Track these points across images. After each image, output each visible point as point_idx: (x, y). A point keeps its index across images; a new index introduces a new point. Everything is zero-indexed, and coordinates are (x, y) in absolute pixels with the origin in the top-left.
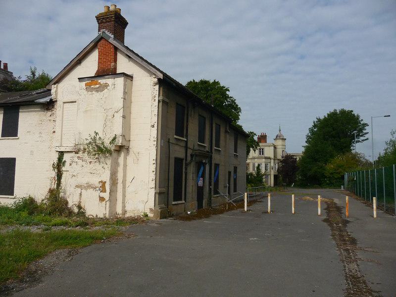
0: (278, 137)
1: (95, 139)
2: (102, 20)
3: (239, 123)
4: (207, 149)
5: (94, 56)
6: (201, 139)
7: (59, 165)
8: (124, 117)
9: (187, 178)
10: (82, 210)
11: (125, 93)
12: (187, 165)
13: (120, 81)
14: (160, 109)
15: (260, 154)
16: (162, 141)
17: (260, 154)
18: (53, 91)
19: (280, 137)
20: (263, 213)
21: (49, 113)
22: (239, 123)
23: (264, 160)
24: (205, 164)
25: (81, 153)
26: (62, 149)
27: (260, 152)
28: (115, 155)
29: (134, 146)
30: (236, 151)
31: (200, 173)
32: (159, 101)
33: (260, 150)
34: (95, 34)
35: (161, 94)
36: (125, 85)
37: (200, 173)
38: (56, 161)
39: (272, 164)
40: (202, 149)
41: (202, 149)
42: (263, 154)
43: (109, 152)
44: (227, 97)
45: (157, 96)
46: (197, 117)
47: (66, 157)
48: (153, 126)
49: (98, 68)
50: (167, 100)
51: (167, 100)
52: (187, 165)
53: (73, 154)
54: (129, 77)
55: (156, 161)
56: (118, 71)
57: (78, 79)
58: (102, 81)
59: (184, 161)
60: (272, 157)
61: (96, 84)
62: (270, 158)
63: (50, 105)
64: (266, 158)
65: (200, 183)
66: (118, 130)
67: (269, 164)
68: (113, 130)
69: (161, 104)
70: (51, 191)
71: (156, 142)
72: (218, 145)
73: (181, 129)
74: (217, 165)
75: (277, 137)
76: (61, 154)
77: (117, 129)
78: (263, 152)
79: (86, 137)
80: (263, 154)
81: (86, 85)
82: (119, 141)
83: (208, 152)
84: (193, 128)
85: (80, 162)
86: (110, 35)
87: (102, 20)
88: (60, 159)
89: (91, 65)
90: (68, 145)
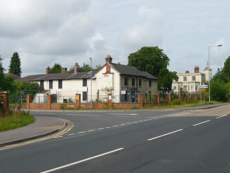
0: (206, 69)
1: (106, 88)
2: (107, 59)
5: (105, 68)
6: (133, 84)
7: (98, 93)
8: (112, 83)
10: (140, 62)
11: (113, 77)
13: (112, 74)
15: (193, 80)
17: (193, 80)
18: (96, 75)
19: (207, 68)
21: (95, 81)
24: (135, 92)
25: (103, 91)
26: (99, 90)
27: (193, 79)
28: (111, 91)
29: (115, 89)
31: (133, 94)
33: (193, 77)
34: (105, 63)
37: (133, 94)
38: (97, 92)
42: (195, 80)
43: (110, 90)
44: (162, 54)
46: (131, 79)
47: (99, 91)
50: (122, 78)
51: (122, 78)
53: (101, 91)
56: (111, 72)
58: (107, 75)
60: (200, 81)
62: (199, 83)
63: (95, 79)
64: (196, 82)
65: (133, 97)
66: (111, 86)
68: (110, 86)
70: (96, 99)
72: (140, 85)
73: (126, 84)
75: (206, 68)
76: (98, 91)
77: (111, 85)
78: (195, 79)
79: (105, 87)
80: (195, 80)
82: (112, 88)
84: (130, 82)
87: (107, 59)
88: (98, 92)
89: (104, 70)
90: (100, 88)
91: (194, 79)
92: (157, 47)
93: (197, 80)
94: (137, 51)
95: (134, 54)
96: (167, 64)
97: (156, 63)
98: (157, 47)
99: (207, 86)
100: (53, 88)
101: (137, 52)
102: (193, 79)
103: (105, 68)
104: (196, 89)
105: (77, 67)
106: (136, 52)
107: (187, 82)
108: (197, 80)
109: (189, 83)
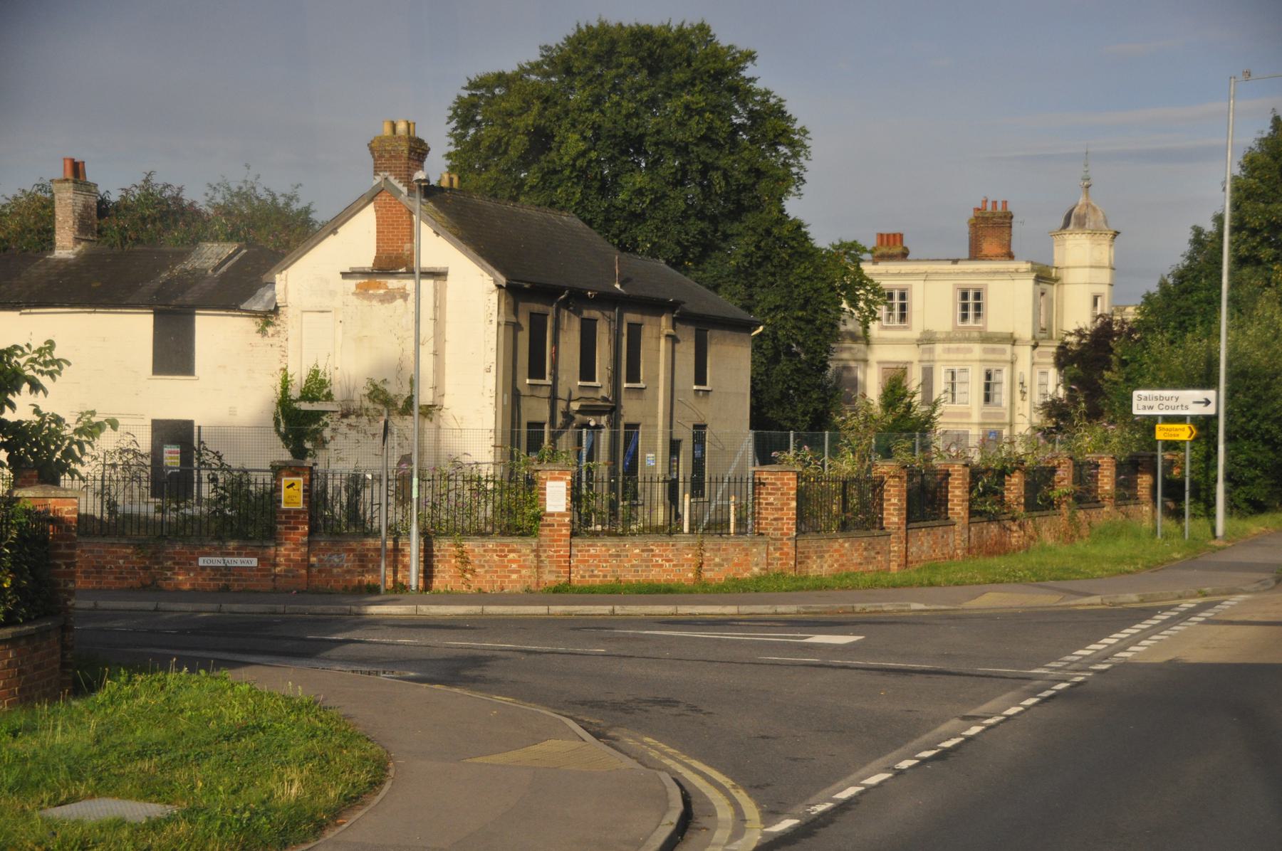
3: (793, 207)
4: (604, 393)
5: (366, 220)
8: (435, 354)
9: (443, 630)
12: (555, 437)
13: (427, 285)
14: (501, 338)
15: (965, 317)
16: (506, 396)
20: (220, 367)
22: (793, 207)
23: (977, 350)
30: (700, 378)
32: (499, 324)
35: (502, 310)
36: (435, 287)
39: (1024, 366)
40: (590, 394)
41: (590, 394)
44: (741, 91)
45: (495, 313)
48: (489, 371)
49: (378, 250)
52: (555, 437)
54: (438, 275)
55: (495, 432)
57: (342, 273)
58: (393, 283)
59: (547, 428)
60: (1025, 331)
61: (378, 288)
62: (1012, 340)
64: (987, 338)
67: (1006, 371)
69: (502, 328)
71: (494, 399)
72: (633, 376)
74: (633, 427)
80: (978, 315)
81: (358, 286)
83: (605, 399)
85: (353, 434)
86: (400, 186)
91: (971, 301)
92: (703, 29)
93: (995, 321)
94: (535, 57)
95: (501, 79)
96: (785, 180)
97: (479, 118)
98: (703, 29)
99: (1207, 402)
100: (190, 419)
101: (535, 67)
102: (965, 307)
103: (366, 220)
104: (987, 398)
105: (80, 199)
106: (522, 68)
107: (915, 332)
108: (995, 321)
109: (928, 339)
